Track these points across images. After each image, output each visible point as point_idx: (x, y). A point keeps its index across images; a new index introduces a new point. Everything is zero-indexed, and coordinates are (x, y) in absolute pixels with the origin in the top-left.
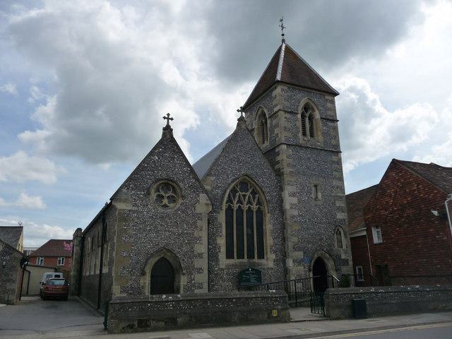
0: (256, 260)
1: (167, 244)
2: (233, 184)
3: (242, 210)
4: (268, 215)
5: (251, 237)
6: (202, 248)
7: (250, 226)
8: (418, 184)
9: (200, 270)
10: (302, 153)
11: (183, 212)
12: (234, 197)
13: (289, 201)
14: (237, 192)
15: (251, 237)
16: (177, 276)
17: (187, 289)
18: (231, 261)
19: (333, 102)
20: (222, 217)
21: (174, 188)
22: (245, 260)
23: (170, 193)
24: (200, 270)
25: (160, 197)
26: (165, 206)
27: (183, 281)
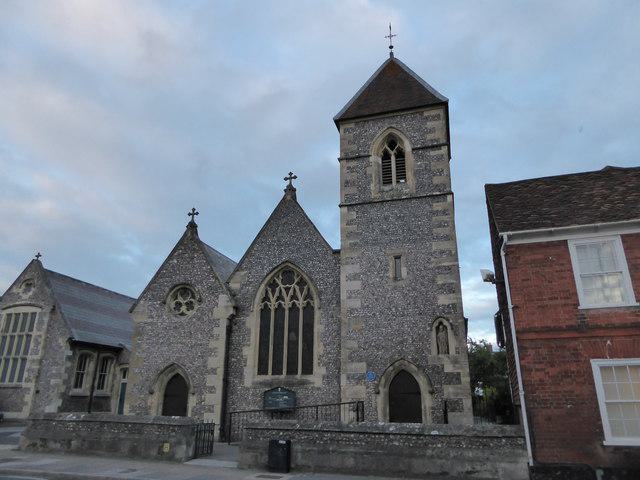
0: (299, 376)
2: (270, 276)
3: (284, 309)
5: (293, 345)
7: (293, 329)
9: (212, 389)
10: (373, 212)
12: (273, 292)
15: (293, 345)
17: (197, 412)
18: (263, 378)
20: (252, 322)
23: (189, 299)
24: (212, 389)
25: (179, 305)
26: (182, 314)
27: (192, 402)
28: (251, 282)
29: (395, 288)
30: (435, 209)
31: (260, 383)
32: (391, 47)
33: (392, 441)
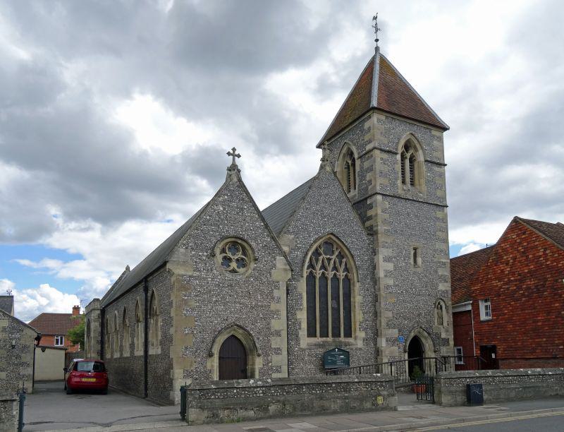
0: (342, 339)
1: (238, 319)
4: (358, 285)
5: (336, 311)
6: (279, 324)
7: (336, 297)
8: (545, 251)
10: (401, 204)
11: (256, 279)
12: (317, 260)
13: (384, 267)
14: (320, 254)
15: (336, 311)
16: (250, 357)
18: (313, 340)
19: (441, 139)
21: (244, 249)
22: (330, 339)
23: (240, 255)
26: (234, 271)
27: (258, 363)
28: (299, 248)
29: (414, 273)
30: (438, 216)
31: (315, 345)
32: (377, 40)
33: (531, 379)
